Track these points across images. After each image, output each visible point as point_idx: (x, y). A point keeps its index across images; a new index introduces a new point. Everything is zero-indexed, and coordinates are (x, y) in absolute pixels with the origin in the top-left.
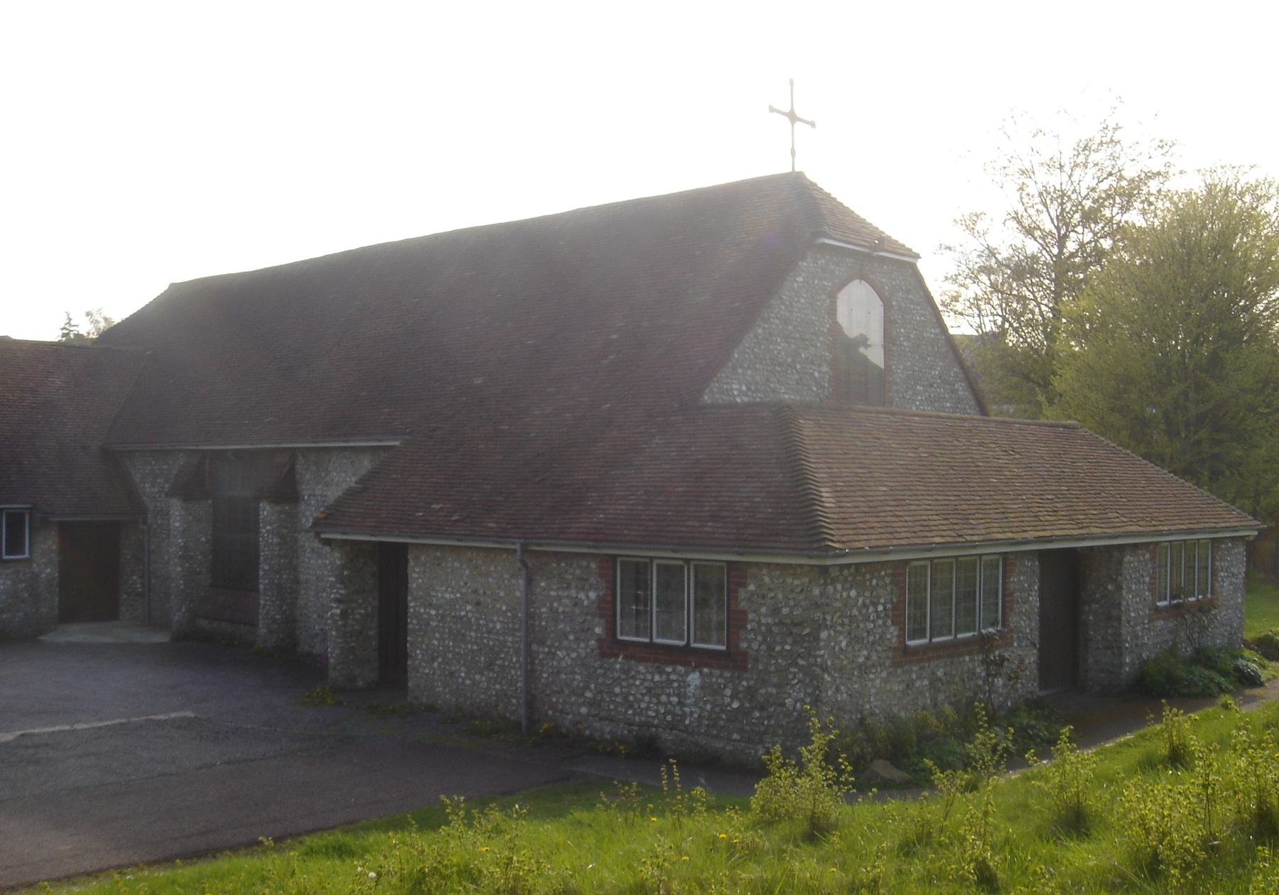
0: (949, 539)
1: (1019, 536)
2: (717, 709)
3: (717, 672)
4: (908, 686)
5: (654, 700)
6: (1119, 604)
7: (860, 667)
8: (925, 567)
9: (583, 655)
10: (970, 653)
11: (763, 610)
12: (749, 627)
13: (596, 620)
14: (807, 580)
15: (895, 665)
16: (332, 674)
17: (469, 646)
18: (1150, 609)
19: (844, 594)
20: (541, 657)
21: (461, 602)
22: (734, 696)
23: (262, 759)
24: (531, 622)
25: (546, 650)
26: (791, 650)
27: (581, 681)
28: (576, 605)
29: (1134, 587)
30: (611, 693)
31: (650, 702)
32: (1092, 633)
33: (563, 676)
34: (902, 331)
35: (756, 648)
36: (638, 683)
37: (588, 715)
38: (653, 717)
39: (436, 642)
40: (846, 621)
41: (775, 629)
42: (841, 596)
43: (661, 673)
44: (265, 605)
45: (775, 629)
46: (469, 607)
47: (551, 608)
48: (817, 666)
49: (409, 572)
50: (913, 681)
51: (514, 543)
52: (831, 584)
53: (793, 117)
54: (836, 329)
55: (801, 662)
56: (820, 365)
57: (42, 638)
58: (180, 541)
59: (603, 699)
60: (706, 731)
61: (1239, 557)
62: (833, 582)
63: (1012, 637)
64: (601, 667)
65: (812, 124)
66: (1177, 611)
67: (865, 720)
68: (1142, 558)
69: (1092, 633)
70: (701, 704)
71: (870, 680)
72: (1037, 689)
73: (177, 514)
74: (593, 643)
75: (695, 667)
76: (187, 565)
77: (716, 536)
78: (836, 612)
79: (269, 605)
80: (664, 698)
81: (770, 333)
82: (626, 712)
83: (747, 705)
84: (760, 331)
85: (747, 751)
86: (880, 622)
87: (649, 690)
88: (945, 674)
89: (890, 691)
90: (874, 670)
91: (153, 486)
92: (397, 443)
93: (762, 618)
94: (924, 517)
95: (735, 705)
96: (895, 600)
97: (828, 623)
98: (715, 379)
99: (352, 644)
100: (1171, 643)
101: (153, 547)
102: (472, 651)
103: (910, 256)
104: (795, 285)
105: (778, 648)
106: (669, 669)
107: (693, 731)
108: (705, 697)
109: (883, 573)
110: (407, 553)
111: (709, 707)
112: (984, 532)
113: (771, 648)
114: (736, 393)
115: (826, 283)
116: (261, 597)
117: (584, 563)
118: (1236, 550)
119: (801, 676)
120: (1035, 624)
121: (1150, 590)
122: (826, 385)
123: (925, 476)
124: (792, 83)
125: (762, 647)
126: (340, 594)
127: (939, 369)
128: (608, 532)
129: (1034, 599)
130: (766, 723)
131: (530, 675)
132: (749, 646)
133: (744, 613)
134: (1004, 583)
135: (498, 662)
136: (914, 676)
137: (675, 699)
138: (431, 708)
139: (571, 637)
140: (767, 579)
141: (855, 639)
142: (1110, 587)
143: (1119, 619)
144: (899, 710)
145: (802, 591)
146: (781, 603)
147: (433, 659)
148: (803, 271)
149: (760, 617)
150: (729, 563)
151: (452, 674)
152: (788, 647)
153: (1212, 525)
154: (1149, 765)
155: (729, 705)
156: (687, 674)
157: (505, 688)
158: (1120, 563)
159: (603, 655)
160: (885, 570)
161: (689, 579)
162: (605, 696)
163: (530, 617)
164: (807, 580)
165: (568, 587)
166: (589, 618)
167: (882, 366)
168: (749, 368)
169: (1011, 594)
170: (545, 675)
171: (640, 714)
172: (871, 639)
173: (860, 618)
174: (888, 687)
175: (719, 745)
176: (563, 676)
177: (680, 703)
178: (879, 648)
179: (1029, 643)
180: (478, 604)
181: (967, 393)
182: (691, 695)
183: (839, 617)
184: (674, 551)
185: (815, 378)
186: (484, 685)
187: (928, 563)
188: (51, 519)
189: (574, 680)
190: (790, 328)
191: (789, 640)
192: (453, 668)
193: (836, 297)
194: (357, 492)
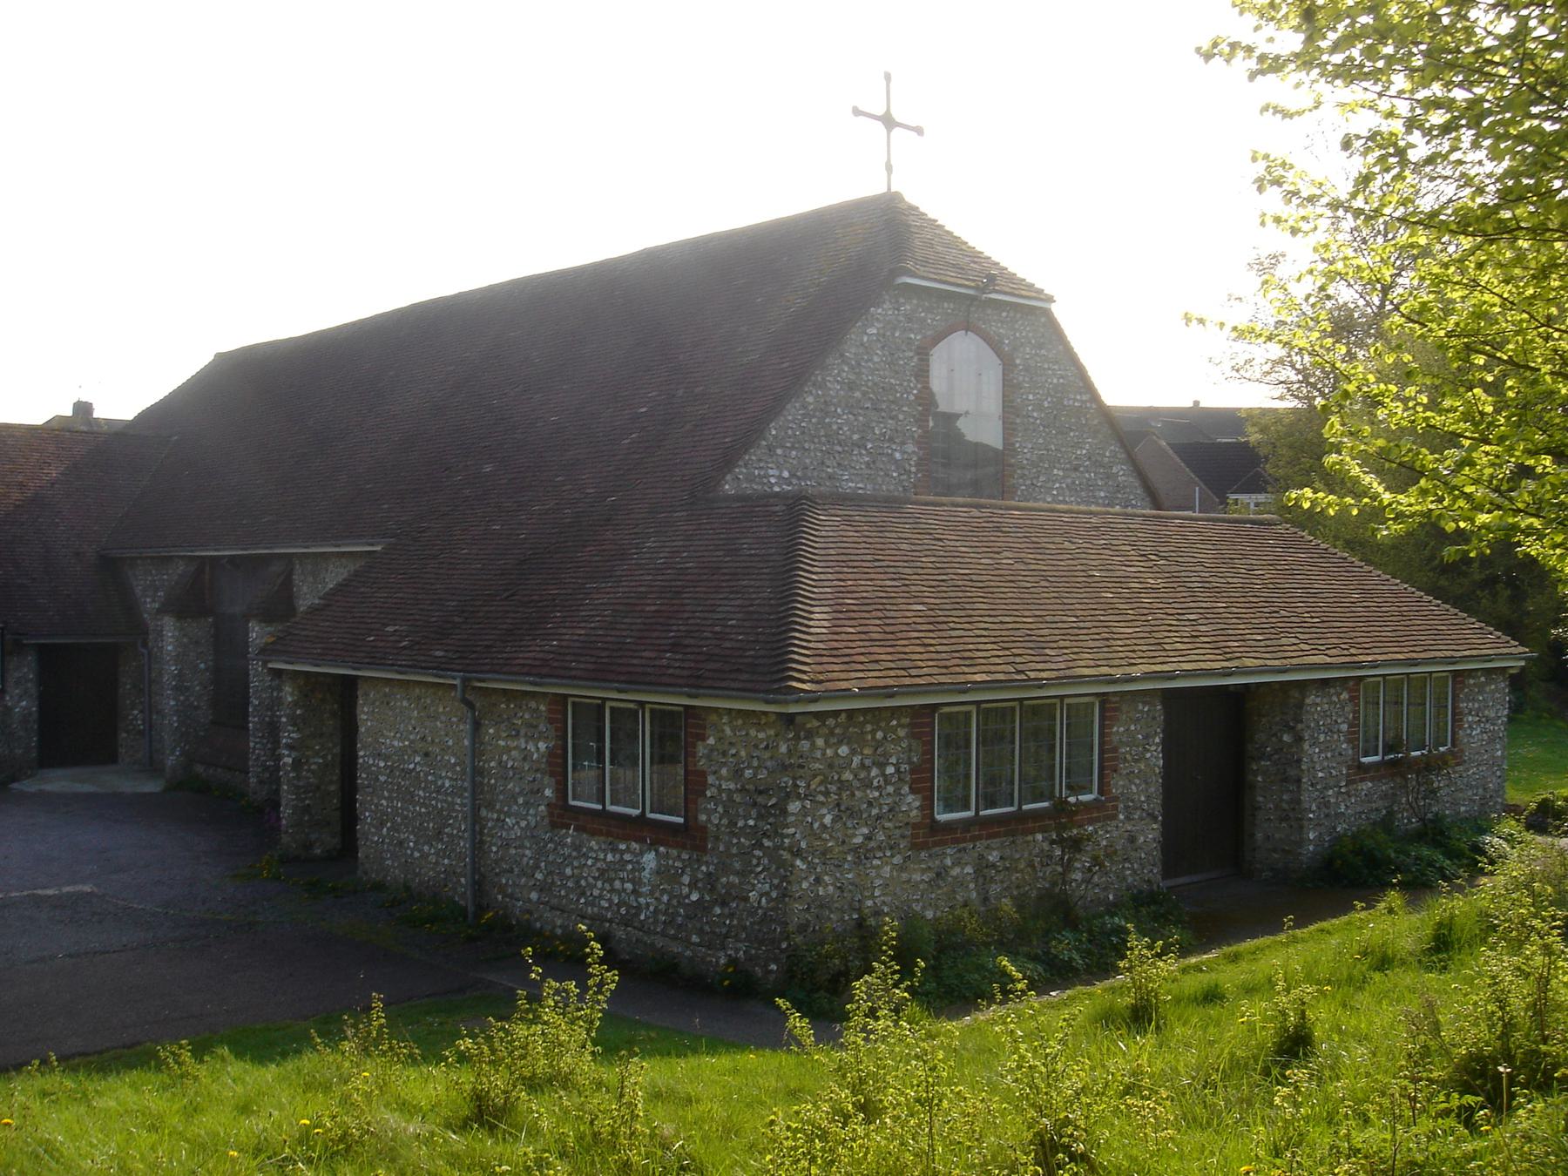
0: (1001, 677)
1: (1118, 673)
2: (675, 902)
3: (674, 852)
4: (938, 874)
5: (607, 886)
6: (1299, 761)
7: (855, 850)
8: (968, 715)
9: (533, 824)
10: (1043, 830)
11: (724, 771)
12: (709, 794)
13: (546, 780)
14: (772, 732)
15: (916, 847)
16: (285, 839)
17: (418, 808)
18: (1349, 768)
19: (829, 752)
20: (490, 825)
21: (409, 752)
22: (693, 885)
23: (122, 951)
24: (478, 779)
25: (495, 816)
26: (755, 825)
27: (531, 858)
28: (525, 759)
29: (1322, 738)
30: (562, 875)
31: (602, 889)
32: (1261, 799)
33: (513, 851)
34: (1031, 397)
35: (717, 822)
36: (589, 862)
37: (539, 902)
38: (607, 909)
39: (384, 802)
40: (833, 788)
41: (737, 798)
42: (824, 754)
43: (615, 850)
44: (254, 748)
45: (737, 798)
46: (418, 759)
47: (500, 762)
48: (784, 850)
49: (358, 712)
50: (945, 868)
51: (454, 678)
52: (806, 738)
53: (888, 121)
54: (927, 400)
55: (767, 843)
56: (903, 443)
57: (15, 785)
58: (173, 668)
59: (553, 882)
60: (662, 930)
61: (1497, 695)
62: (810, 735)
63: (1116, 808)
64: (551, 840)
65: (919, 131)
66: (1394, 768)
67: (865, 920)
68: (1335, 699)
69: (1261, 799)
70: (657, 895)
71: (873, 867)
72: (1159, 877)
73: (170, 636)
74: (542, 808)
75: (651, 844)
76: (182, 698)
77: (671, 671)
78: (815, 776)
79: (259, 749)
80: (617, 884)
81: (825, 402)
82: (578, 900)
83: (707, 898)
84: (810, 399)
85: (708, 959)
86: (890, 789)
87: (602, 872)
88: (1001, 858)
89: (909, 881)
90: (880, 854)
91: (154, 601)
92: (378, 548)
93: (722, 782)
94: (971, 646)
95: (695, 897)
96: (915, 759)
97: (801, 791)
98: (740, 463)
99: (307, 802)
100: (1384, 812)
101: (153, 675)
102: (420, 814)
103: (1041, 300)
104: (865, 339)
105: (740, 824)
106: (623, 847)
107: (649, 928)
108: (661, 884)
109: (894, 722)
110: (356, 690)
111: (665, 898)
112: (1062, 666)
113: (733, 824)
114: (773, 480)
115: (912, 336)
116: (251, 739)
117: (533, 704)
118: (1493, 687)
119: (766, 861)
120: (1155, 788)
121: (1349, 741)
122: (913, 469)
123: (995, 590)
124: (888, 77)
125: (722, 822)
126: (291, 738)
127: (1087, 446)
128: (555, 664)
129: (1155, 756)
130: (728, 922)
131: (478, 846)
132: (709, 820)
133: (703, 774)
134: (1102, 735)
135: (446, 830)
136: (948, 862)
137: (629, 886)
138: (379, 887)
139: (521, 801)
140: (728, 731)
141: (845, 812)
142: (1286, 738)
143: (1299, 781)
144: (924, 908)
145: (767, 747)
146: (743, 763)
147: (382, 824)
148: (877, 319)
149: (721, 782)
150: (686, 707)
151: (401, 843)
152: (751, 822)
153: (1448, 654)
154: (1106, 1018)
155: (688, 896)
156: (642, 853)
157: (454, 863)
158: (1300, 705)
159: (554, 826)
160: (898, 719)
161: (646, 729)
162: (556, 878)
163: (478, 772)
164: (772, 732)
165: (517, 735)
166: (539, 775)
167: (1001, 448)
168: (793, 448)
169: (1115, 750)
170: (494, 849)
171: (593, 905)
172: (875, 812)
173: (856, 783)
174: (905, 876)
175: (676, 948)
176: (513, 851)
177: (634, 891)
178: (888, 825)
179: (1144, 815)
180: (427, 755)
181: (1131, 479)
182: (646, 881)
183: (821, 783)
184: (620, 691)
185: (896, 461)
186: (433, 859)
187: (973, 709)
188: (25, 642)
189: (524, 855)
190: (857, 394)
191: (754, 813)
192: (402, 836)
193: (927, 354)
194: (317, 610)
